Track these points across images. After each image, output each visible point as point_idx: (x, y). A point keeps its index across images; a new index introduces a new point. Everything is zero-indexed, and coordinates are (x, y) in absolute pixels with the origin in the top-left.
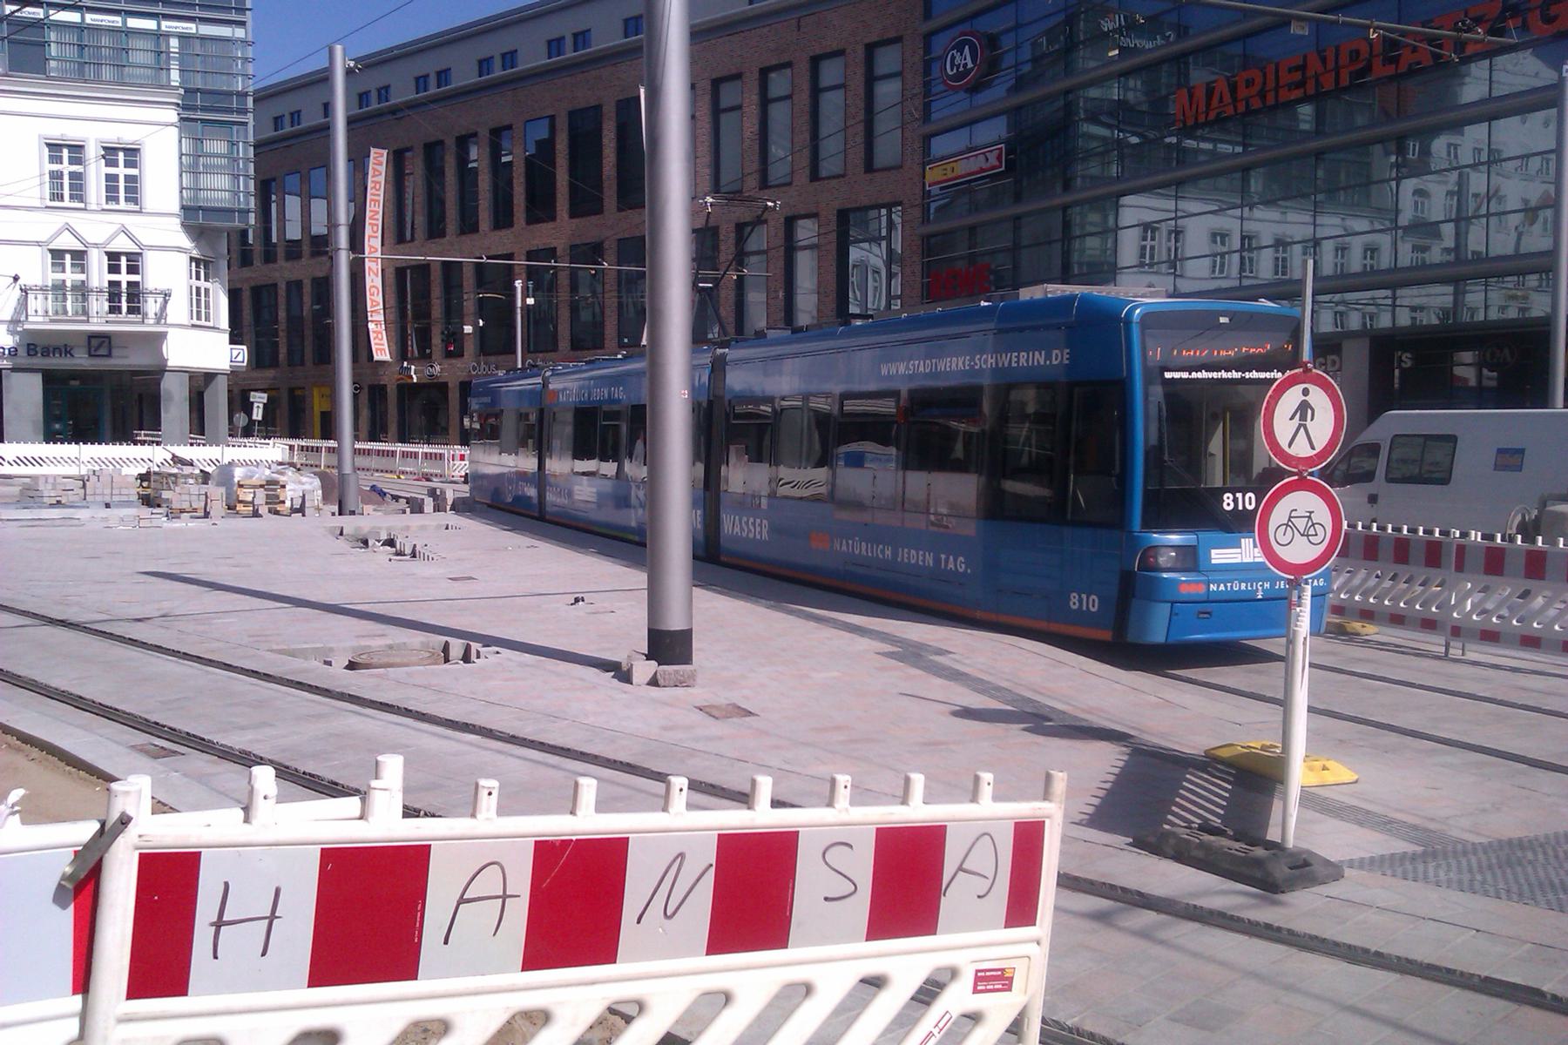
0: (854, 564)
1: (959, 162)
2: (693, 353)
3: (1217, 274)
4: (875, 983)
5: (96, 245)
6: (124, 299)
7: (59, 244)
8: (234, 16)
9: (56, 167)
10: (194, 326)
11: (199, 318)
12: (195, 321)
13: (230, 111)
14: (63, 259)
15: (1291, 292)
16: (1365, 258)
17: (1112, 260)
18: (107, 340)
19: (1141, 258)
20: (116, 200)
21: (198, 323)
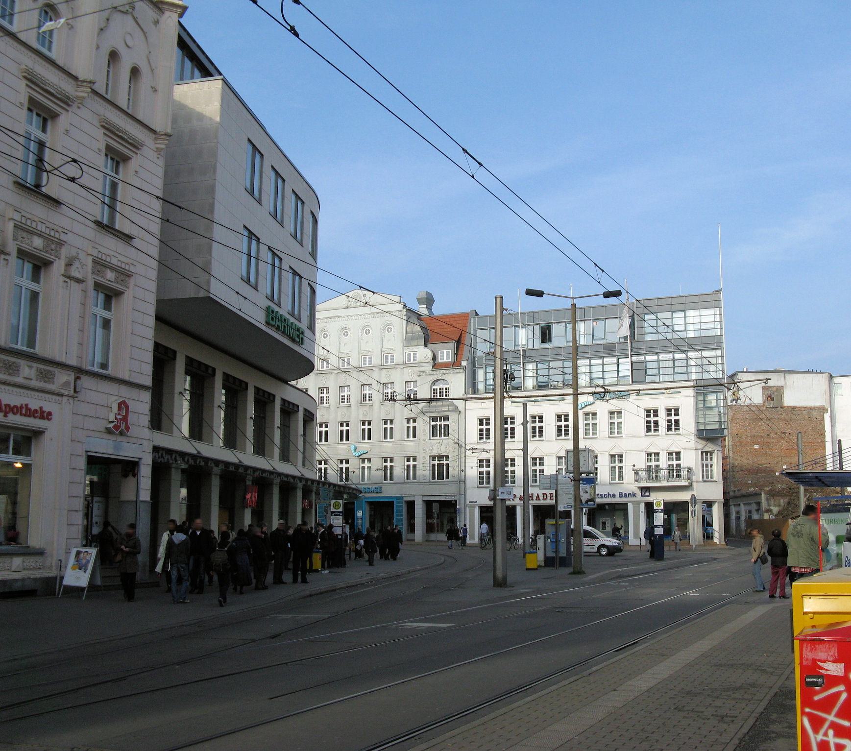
5: (663, 450)
8: (715, 346)
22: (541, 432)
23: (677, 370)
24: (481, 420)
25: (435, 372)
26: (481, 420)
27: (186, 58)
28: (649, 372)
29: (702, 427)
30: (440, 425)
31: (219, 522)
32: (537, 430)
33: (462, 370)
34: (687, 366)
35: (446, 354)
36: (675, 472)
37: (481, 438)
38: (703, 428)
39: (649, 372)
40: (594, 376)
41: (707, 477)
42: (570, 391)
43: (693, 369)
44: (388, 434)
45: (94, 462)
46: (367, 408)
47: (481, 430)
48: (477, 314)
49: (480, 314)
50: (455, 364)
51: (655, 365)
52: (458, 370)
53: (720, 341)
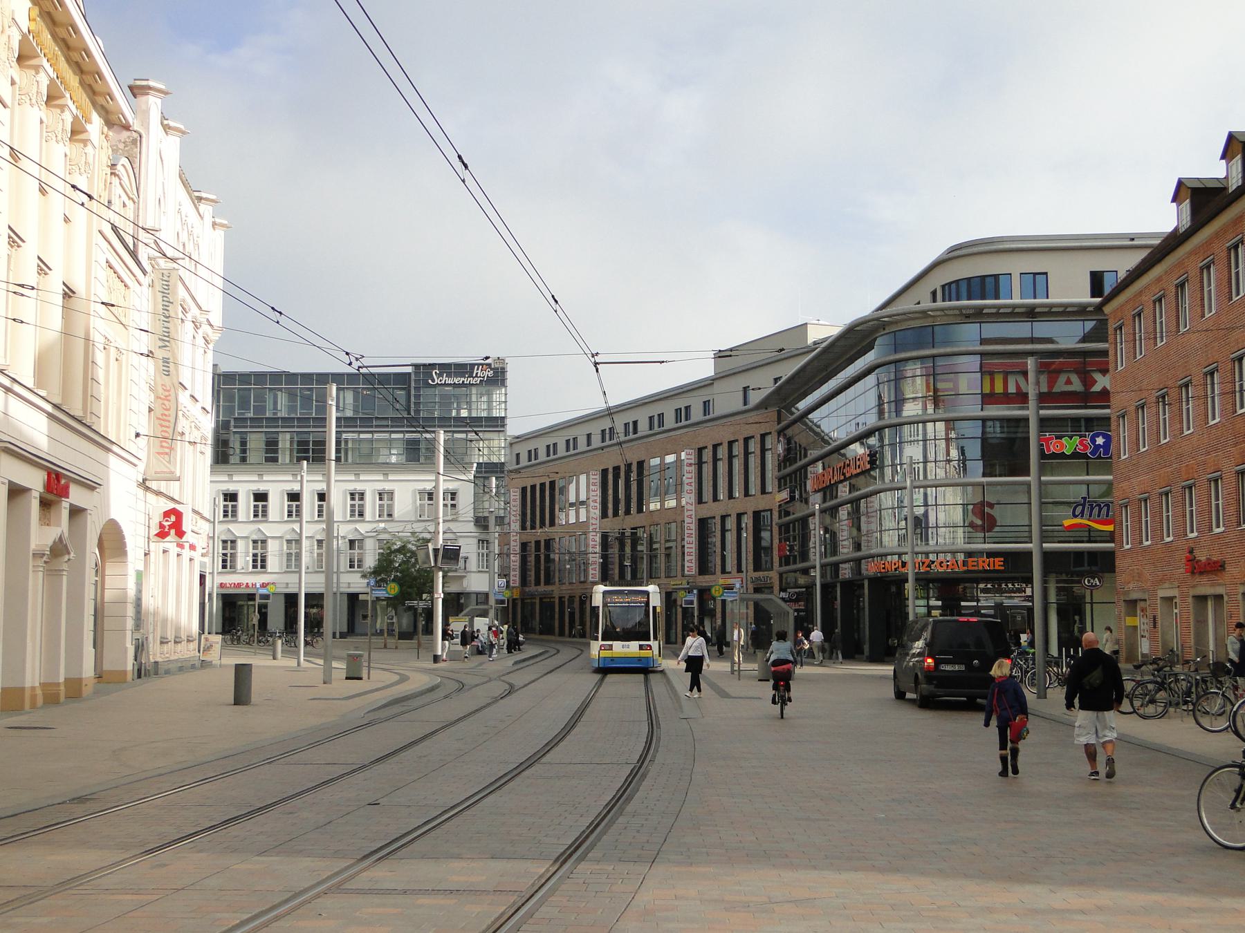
0: (1155, 627)
1: (140, 864)
2: (348, 594)
3: (656, 429)
4: (547, 651)
6: (293, 556)
7: (255, 537)
9: (353, 502)
10: (479, 572)
11: (483, 568)
12: (481, 569)
13: (497, 426)
14: (292, 544)
15: (1022, 398)
16: (479, 549)
17: (1108, 533)
18: (784, 576)
19: (235, 553)
20: (227, 516)
21: (483, 570)
42: (481, 367)
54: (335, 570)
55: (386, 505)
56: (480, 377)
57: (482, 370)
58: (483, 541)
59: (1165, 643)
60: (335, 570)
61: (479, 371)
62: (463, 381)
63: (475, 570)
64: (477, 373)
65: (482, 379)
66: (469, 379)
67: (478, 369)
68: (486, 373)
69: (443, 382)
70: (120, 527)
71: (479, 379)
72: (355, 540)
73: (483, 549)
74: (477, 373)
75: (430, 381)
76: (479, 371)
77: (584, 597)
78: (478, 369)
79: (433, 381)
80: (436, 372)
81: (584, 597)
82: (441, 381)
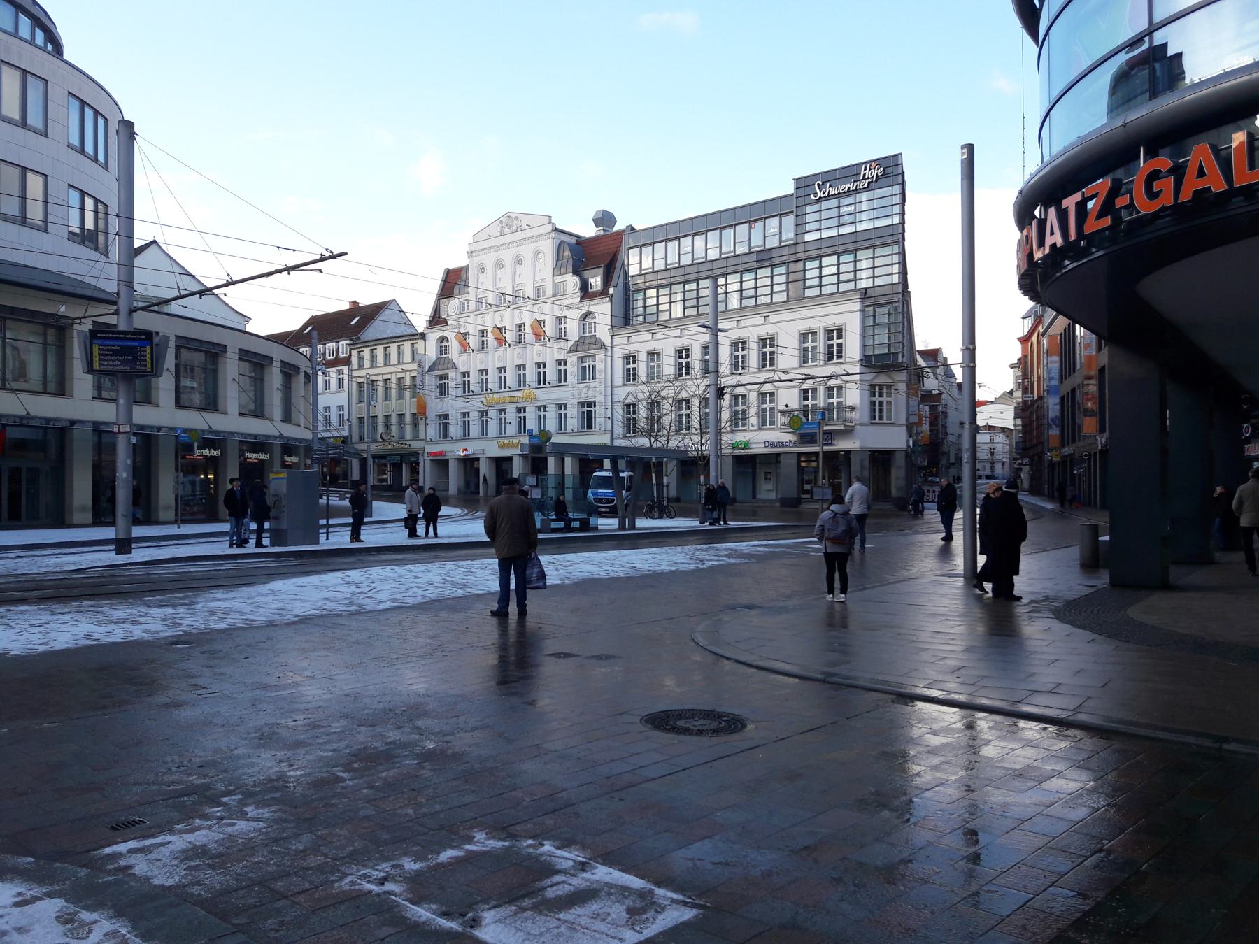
2: (870, 451)
3: (542, 386)
22: (840, 352)
23: (842, 277)
24: (680, 351)
25: (585, 303)
26: (680, 351)
27: (36, 29)
28: (808, 283)
29: (869, 352)
30: (589, 366)
31: (1015, 414)
32: (768, 357)
33: (608, 299)
34: (855, 271)
35: (596, 282)
36: (695, 422)
37: (628, 380)
38: (871, 353)
39: (808, 283)
40: (745, 294)
41: (881, 418)
42: (407, 345)
43: (863, 274)
44: (562, 377)
45: (359, 418)
46: (541, 348)
47: (764, 354)
48: (633, 229)
49: (638, 228)
50: (603, 293)
51: (694, 294)
52: (604, 300)
53: (9, 329)
54: (331, 521)
55: (835, 337)
56: (868, 178)
57: (870, 169)
58: (881, 387)
59: (959, 616)
60: (331, 521)
61: (867, 171)
62: (849, 188)
63: (866, 422)
64: (865, 174)
65: (870, 180)
66: (855, 184)
67: (865, 169)
68: (875, 172)
69: (826, 194)
70: (1019, 283)
71: (867, 181)
72: (808, 389)
73: (881, 395)
74: (865, 174)
75: (812, 196)
76: (867, 171)
77: (1086, 455)
78: (865, 169)
79: (815, 194)
80: (818, 184)
81: (1086, 455)
82: (824, 193)
